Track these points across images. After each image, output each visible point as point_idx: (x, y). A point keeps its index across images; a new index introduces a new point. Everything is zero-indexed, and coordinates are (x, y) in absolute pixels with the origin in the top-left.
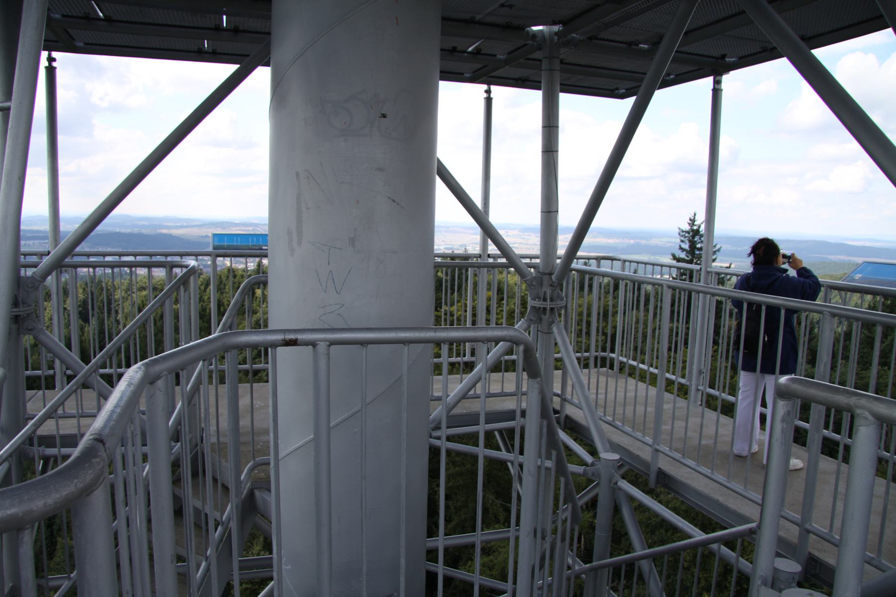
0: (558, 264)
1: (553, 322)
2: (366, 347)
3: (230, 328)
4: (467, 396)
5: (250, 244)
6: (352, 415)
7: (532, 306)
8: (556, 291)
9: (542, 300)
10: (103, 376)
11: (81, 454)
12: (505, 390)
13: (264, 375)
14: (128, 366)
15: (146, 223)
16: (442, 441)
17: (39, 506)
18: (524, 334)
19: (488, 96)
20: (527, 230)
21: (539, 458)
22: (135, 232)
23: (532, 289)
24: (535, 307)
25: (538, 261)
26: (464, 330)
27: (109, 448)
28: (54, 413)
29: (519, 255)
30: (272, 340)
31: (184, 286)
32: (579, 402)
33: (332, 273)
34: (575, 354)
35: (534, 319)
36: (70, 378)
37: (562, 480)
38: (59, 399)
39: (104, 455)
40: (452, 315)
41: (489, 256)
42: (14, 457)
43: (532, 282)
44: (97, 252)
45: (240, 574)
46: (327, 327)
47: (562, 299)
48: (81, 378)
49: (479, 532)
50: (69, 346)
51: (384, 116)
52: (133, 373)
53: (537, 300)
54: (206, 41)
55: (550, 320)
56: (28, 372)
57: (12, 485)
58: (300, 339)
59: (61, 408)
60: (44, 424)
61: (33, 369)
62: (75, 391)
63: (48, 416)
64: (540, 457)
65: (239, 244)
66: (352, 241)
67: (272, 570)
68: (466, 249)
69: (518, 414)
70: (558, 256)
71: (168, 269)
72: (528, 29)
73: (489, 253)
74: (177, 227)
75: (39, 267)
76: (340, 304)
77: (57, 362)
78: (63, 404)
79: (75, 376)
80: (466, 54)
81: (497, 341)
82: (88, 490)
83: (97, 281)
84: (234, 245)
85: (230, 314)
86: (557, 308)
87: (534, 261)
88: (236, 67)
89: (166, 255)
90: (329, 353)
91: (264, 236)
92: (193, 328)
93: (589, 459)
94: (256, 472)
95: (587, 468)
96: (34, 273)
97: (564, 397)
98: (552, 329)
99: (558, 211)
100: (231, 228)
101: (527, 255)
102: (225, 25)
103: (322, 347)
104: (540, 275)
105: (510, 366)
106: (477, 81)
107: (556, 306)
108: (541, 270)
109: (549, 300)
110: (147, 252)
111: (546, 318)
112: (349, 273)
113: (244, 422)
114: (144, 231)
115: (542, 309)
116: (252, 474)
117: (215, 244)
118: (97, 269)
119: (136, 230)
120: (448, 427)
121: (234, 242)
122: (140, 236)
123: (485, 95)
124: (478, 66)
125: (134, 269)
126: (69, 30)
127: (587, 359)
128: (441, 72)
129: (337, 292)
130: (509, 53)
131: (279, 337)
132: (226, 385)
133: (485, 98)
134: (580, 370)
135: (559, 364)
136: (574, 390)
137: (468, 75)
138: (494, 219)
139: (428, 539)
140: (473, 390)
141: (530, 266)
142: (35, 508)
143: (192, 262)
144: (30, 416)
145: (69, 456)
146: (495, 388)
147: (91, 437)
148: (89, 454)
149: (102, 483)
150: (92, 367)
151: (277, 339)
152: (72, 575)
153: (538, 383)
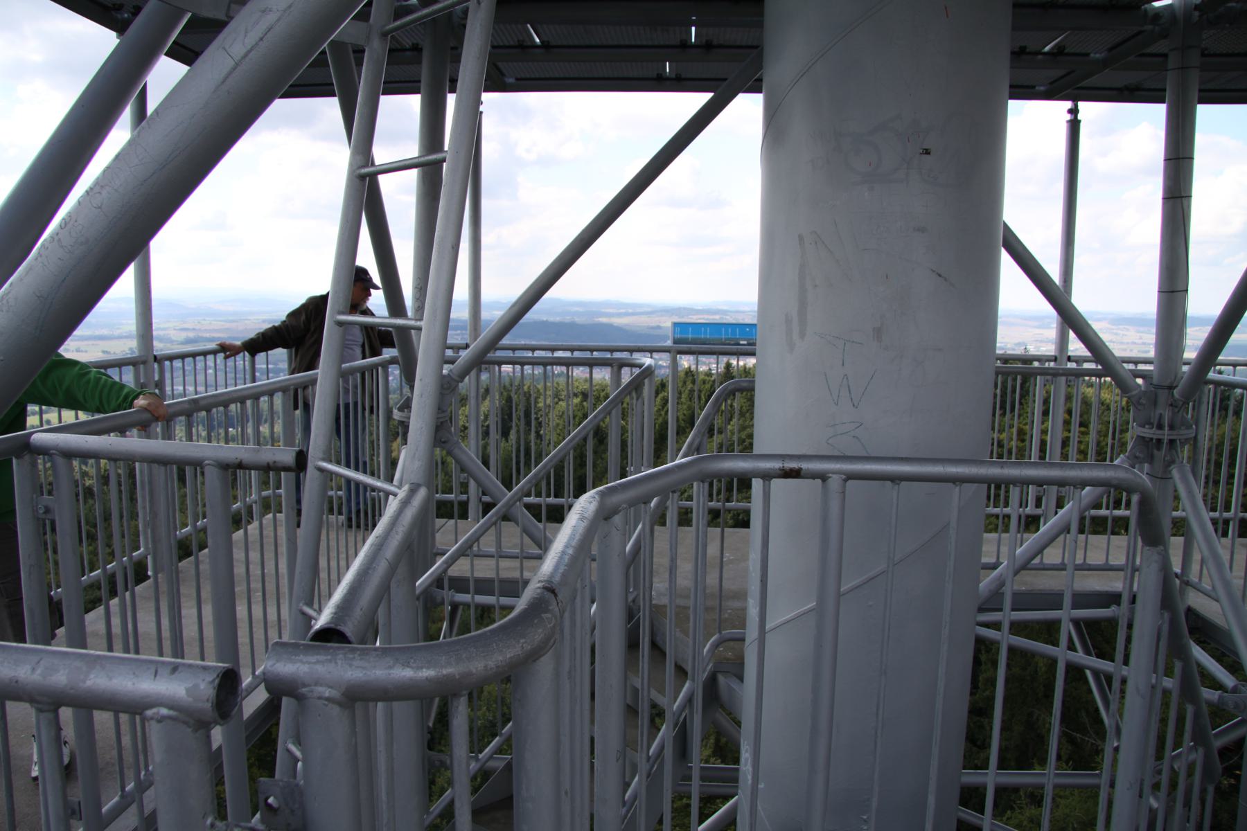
0: (1184, 373)
1: (1173, 462)
2: (899, 484)
3: (698, 450)
4: (1029, 566)
5: (723, 337)
6: (868, 581)
7: (1138, 436)
8: (1180, 413)
9: (1155, 427)
10: (528, 507)
11: (529, 606)
12: (1089, 561)
13: (729, 518)
14: (580, 490)
15: (581, 310)
16: (1003, 634)
17: (479, 669)
18: (1141, 477)
19: (1073, 117)
20: (1136, 322)
21: (1154, 673)
22: (567, 321)
23: (1139, 410)
24: (1143, 438)
25: (1150, 367)
26: (1045, 467)
27: (562, 602)
28: (469, 550)
29: (1121, 358)
30: (765, 469)
31: (636, 392)
32: (1213, 588)
33: (847, 378)
34: (1208, 514)
35: (1141, 456)
36: (487, 508)
37: (1190, 709)
38: (475, 532)
39: (557, 609)
40: (1000, 445)
41: (1069, 359)
42: (421, 599)
43: (1140, 398)
44: (525, 344)
45: (701, 786)
46: (836, 453)
47: (1189, 427)
48: (503, 506)
49: (1052, 771)
50: (486, 463)
51: (927, 152)
52: (584, 506)
53: (1147, 426)
54: (668, 63)
55: (1168, 458)
56: (437, 495)
57: (470, 632)
58: (805, 470)
59: (476, 544)
60: (457, 562)
61: (443, 492)
62: (495, 523)
63: (462, 553)
64: (1155, 671)
65: (708, 337)
66: (878, 333)
67: (737, 786)
68: (1026, 348)
69: (1125, 598)
70: (1184, 361)
71: (615, 368)
72: (1146, 6)
73: (1070, 354)
74: (619, 315)
75: (456, 363)
76: (858, 422)
77: (472, 484)
78: (477, 540)
79: (494, 505)
80: (1040, 57)
81: (1083, 484)
82: (534, 655)
83: (517, 384)
84: (700, 339)
85: (699, 431)
86: (1180, 440)
87: (1141, 367)
88: (706, 97)
89: (612, 350)
90: (845, 490)
91: (753, 326)
92: (645, 449)
93: (1228, 680)
94: (721, 649)
95: (1225, 694)
96: (451, 370)
97: (1185, 578)
98: (1170, 472)
99: (1187, 290)
100: (690, 316)
101: (1130, 358)
102: (693, 40)
103: (835, 482)
104: (1153, 389)
105: (1120, 526)
106: (1056, 97)
107: (1180, 437)
108: (1155, 381)
109: (1166, 428)
110: (587, 346)
111: (1160, 455)
112: (872, 378)
113: (712, 579)
114: (578, 320)
115: (1154, 441)
116: (716, 651)
117: (676, 336)
118: (526, 367)
119: (568, 318)
120: (1013, 610)
121: (701, 334)
122: (572, 326)
123: (1068, 117)
124: (1061, 72)
125: (549, 368)
126: (499, 64)
127: (1226, 522)
128: (1011, 87)
129: (854, 405)
130: (1110, 50)
131: (776, 465)
132: (692, 529)
133: (1068, 122)
134: (1216, 538)
135: (1180, 527)
136: (1204, 568)
137: (1042, 88)
138: (1081, 300)
139: (963, 771)
140: (1039, 556)
141: (1137, 374)
142: (474, 671)
143: (647, 361)
144: (440, 551)
145: (511, 608)
146: (1096, 558)
147: (539, 585)
148: (537, 607)
149: (552, 646)
150: (516, 493)
151: (772, 467)
152: (480, 756)
153: (1159, 554)
